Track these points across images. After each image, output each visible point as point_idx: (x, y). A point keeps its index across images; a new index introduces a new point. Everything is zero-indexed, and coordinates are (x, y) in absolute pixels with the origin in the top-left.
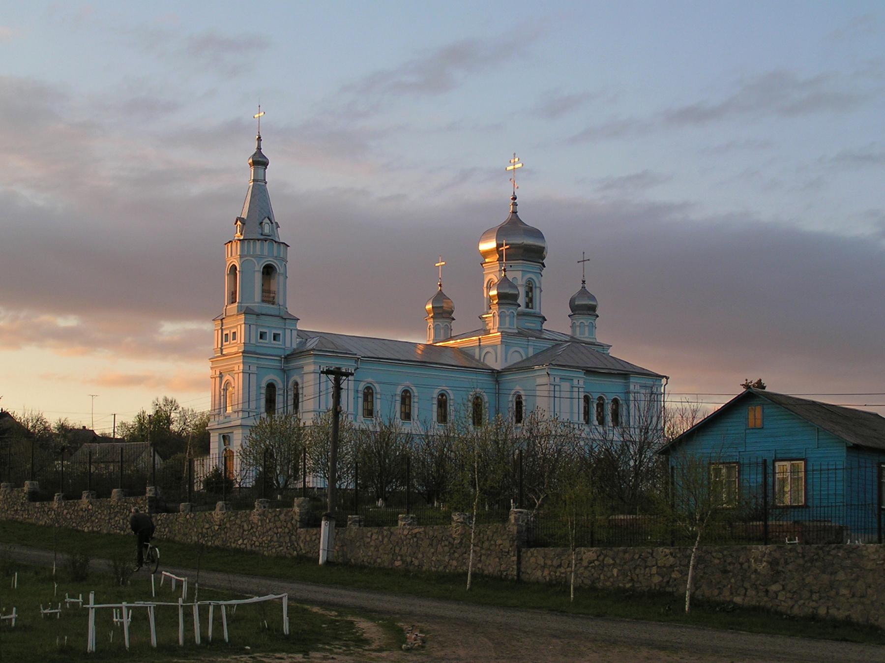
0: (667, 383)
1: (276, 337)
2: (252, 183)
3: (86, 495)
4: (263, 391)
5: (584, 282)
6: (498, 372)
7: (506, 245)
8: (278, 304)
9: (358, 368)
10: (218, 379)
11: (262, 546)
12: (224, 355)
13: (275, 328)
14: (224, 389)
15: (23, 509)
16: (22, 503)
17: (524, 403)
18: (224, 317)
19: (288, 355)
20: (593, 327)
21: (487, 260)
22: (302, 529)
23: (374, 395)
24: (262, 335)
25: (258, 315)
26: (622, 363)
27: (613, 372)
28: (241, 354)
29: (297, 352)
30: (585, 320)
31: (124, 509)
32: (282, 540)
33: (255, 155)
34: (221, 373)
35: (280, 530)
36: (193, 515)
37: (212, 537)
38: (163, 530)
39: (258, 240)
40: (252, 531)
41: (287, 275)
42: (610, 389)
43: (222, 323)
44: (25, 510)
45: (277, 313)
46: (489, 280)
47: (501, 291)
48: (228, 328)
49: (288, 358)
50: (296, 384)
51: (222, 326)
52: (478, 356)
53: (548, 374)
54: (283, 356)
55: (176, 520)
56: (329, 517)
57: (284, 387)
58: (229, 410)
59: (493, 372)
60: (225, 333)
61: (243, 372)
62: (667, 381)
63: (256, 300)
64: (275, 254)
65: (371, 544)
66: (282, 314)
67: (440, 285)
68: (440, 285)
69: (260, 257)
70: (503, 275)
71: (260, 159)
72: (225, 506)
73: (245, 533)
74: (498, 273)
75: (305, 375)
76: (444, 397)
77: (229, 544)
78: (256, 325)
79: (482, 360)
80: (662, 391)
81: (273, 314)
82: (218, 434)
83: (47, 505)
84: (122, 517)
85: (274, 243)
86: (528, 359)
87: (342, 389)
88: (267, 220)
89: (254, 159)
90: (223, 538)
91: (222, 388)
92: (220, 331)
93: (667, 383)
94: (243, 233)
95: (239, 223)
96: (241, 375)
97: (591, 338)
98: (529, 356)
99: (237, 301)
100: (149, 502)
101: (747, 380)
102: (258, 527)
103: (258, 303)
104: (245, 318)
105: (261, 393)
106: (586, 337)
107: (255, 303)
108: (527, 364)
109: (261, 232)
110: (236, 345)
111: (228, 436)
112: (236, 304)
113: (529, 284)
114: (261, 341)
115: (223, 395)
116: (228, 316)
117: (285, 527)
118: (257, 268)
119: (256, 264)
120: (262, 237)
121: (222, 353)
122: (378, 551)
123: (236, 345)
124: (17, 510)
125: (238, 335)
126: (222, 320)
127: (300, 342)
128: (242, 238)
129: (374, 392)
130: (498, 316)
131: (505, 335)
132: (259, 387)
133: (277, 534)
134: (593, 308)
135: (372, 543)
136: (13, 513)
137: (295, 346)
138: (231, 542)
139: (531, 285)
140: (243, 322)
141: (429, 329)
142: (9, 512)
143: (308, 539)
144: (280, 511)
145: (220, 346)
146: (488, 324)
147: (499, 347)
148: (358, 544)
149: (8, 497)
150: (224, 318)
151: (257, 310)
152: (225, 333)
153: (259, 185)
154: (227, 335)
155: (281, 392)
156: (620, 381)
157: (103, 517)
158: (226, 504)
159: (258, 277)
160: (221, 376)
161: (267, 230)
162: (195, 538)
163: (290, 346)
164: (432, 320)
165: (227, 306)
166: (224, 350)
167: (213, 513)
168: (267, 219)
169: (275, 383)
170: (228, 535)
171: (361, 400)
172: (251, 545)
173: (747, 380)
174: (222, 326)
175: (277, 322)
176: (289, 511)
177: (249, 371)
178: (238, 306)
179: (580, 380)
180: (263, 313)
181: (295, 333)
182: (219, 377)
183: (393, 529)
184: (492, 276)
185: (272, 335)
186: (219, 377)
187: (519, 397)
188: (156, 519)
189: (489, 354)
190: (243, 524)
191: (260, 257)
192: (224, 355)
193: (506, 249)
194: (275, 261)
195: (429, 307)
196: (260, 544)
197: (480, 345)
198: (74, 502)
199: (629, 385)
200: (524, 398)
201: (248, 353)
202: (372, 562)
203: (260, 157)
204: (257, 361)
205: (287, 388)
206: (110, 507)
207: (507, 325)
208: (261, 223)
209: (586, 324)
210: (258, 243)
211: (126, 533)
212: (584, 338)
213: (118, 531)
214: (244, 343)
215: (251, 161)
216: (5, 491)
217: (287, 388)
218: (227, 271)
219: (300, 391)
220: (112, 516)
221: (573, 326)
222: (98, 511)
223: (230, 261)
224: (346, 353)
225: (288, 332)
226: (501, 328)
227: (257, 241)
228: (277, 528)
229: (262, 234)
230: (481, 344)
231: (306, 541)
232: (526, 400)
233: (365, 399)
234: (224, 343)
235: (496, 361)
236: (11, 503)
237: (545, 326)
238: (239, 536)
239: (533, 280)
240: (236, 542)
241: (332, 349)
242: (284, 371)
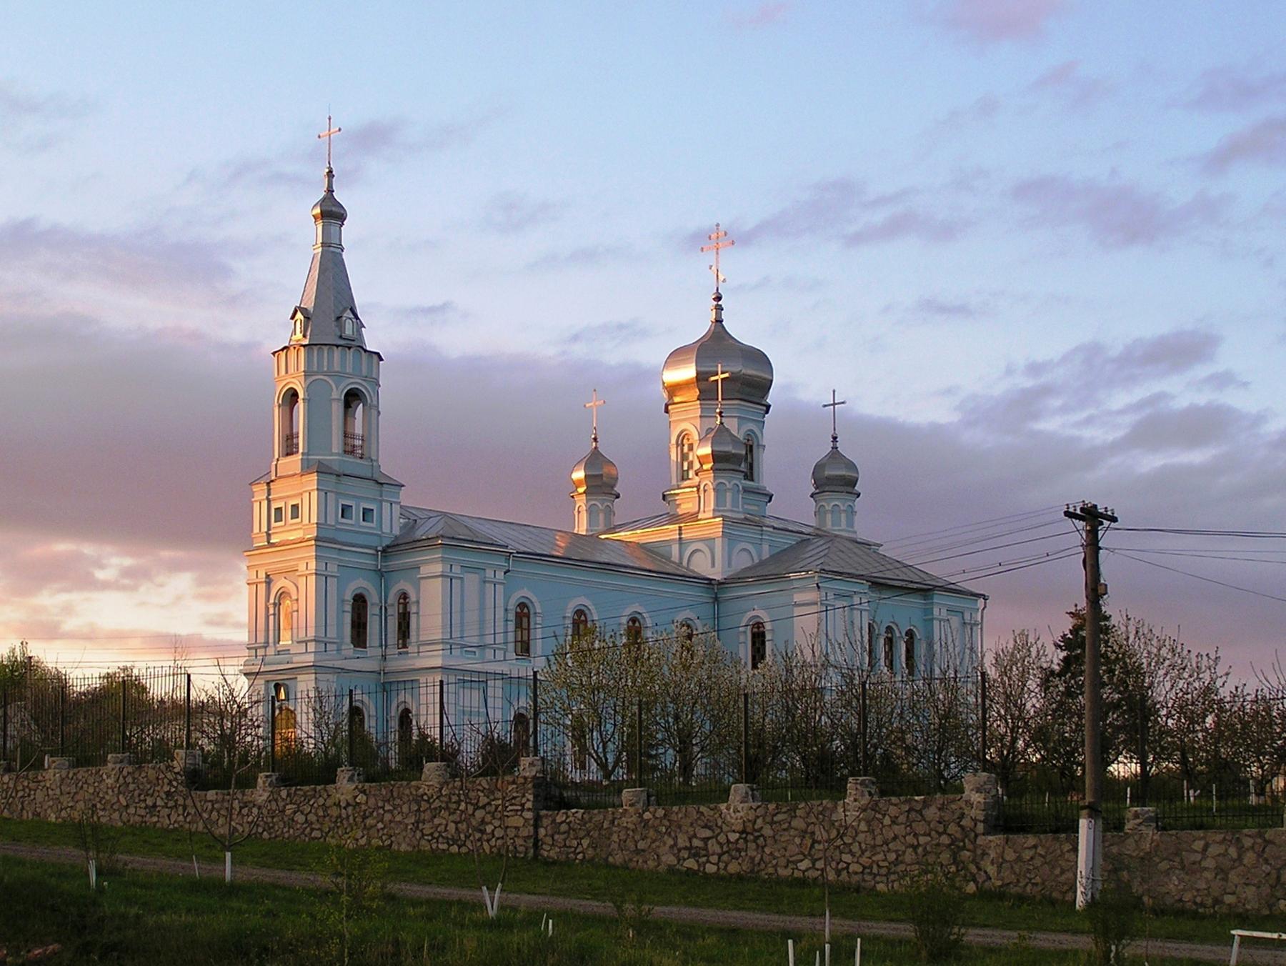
0: (985, 607)
1: (367, 513)
2: (320, 250)
3: (347, 776)
4: (348, 608)
5: (835, 438)
6: (720, 583)
7: (722, 373)
8: (370, 458)
9: (508, 571)
10: (262, 587)
11: (870, 873)
12: (273, 545)
13: (367, 499)
14: (275, 604)
15: (171, 804)
16: (168, 793)
17: (768, 637)
18: (273, 478)
19: (388, 547)
20: (852, 513)
21: (677, 399)
22: (990, 838)
23: (532, 616)
24: (345, 511)
25: (338, 476)
26: (919, 573)
27: (911, 586)
28: (313, 542)
29: (400, 542)
30: (834, 501)
31: (458, 803)
32: (931, 859)
33: (324, 200)
34: (268, 576)
35: (922, 840)
36: (660, 812)
37: (720, 856)
38: (575, 843)
39: (337, 346)
40: (839, 842)
41: (380, 409)
42: (903, 613)
43: (269, 490)
44: (176, 806)
45: (369, 475)
46: (682, 432)
47: (716, 449)
48: (281, 498)
49: (387, 552)
50: (404, 596)
51: (269, 494)
52: (677, 555)
53: (819, 587)
54: (380, 548)
55: (613, 822)
56: (1093, 811)
57: (381, 602)
58: (286, 641)
59: (710, 584)
60: (274, 505)
61: (316, 574)
62: (985, 603)
63: (334, 450)
64: (364, 372)
65: (1204, 864)
66: (375, 477)
67: (595, 439)
68: (595, 439)
69: (339, 376)
70: (718, 422)
71: (334, 209)
72: (750, 793)
73: (816, 846)
74: (699, 420)
75: (422, 582)
76: (637, 624)
77: (771, 870)
78: (337, 493)
79: (685, 563)
80: (979, 619)
81: (362, 475)
82: (263, 682)
83: (240, 796)
84: (451, 818)
85: (363, 352)
86: (762, 563)
87: (1100, 548)
88: (348, 314)
89: (324, 208)
90: (752, 859)
91: (272, 601)
92: (265, 504)
93: (985, 607)
94: (308, 333)
95: (299, 316)
96: (312, 579)
97: (849, 531)
98: (764, 558)
99: (301, 450)
100: (534, 786)
101: (1076, 606)
102: (857, 834)
103: (338, 454)
104: (318, 479)
105: (344, 611)
106: (842, 530)
107: (332, 454)
108: (772, 569)
109: (339, 334)
110: (300, 526)
111: (284, 684)
112: (297, 458)
113: (748, 440)
114: (344, 521)
115: (274, 614)
116: (281, 477)
117: (940, 834)
118: (335, 395)
119: (334, 386)
120: (342, 342)
121: (269, 542)
122: (1225, 879)
123: (300, 526)
124: (155, 806)
125: (305, 510)
126: (268, 484)
127: (405, 525)
128: (306, 342)
129: (532, 612)
130: (714, 489)
131: (728, 523)
132: (342, 601)
133: (915, 848)
134: (853, 482)
135: (1209, 863)
136: (143, 812)
137: (397, 531)
138: (775, 866)
139: (750, 443)
140: (316, 487)
141: (579, 512)
142: (132, 810)
143: (1010, 856)
144: (924, 801)
145: (264, 529)
146: (680, 505)
147: (718, 542)
148: (1164, 865)
149: (129, 780)
150: (272, 481)
151: (336, 468)
152: (274, 505)
153: (333, 252)
154: (279, 510)
155: (377, 611)
156: (917, 600)
157: (398, 818)
158: (753, 790)
159: (337, 409)
160: (269, 581)
161: (349, 330)
162: (669, 859)
163: (389, 531)
164: (584, 497)
165: (278, 460)
166: (272, 537)
167: (723, 807)
168: (349, 311)
169: (365, 593)
170: (767, 850)
171: (511, 626)
172: (838, 872)
173: (1076, 606)
174: (269, 494)
175: (369, 489)
176: (953, 801)
177: (325, 573)
178: (302, 459)
179: (863, 595)
180: (347, 472)
181: (396, 508)
182: (266, 582)
183: (1269, 834)
184: (686, 426)
185: (361, 510)
186: (266, 582)
187: (759, 625)
188: (554, 821)
189: (697, 555)
190: (810, 828)
191: (339, 376)
192: (273, 545)
193: (722, 379)
194: (364, 383)
195: (579, 475)
196: (864, 867)
197: (680, 538)
198: (315, 790)
199: (932, 608)
200: (768, 626)
201: (324, 541)
202: (1209, 902)
203: (334, 205)
204: (338, 555)
205: (386, 602)
206: (418, 799)
207: (728, 506)
208: (339, 318)
209: (842, 508)
210: (337, 352)
211: (464, 850)
212: (839, 530)
213: (445, 846)
214: (317, 523)
215: (318, 211)
216: (121, 771)
217: (386, 602)
218: (277, 399)
219: (413, 609)
220: (427, 816)
221: (819, 512)
222: (383, 808)
223: (284, 383)
224: (492, 545)
225: (386, 506)
226: (719, 511)
227: (335, 348)
228: (916, 835)
229: (341, 337)
230: (683, 536)
231: (1005, 861)
232: (772, 630)
233: (519, 625)
234: (273, 524)
235: (713, 565)
236: (136, 793)
237: (770, 509)
238: (803, 853)
239: (754, 433)
240: (791, 866)
241: (464, 535)
242: (381, 574)
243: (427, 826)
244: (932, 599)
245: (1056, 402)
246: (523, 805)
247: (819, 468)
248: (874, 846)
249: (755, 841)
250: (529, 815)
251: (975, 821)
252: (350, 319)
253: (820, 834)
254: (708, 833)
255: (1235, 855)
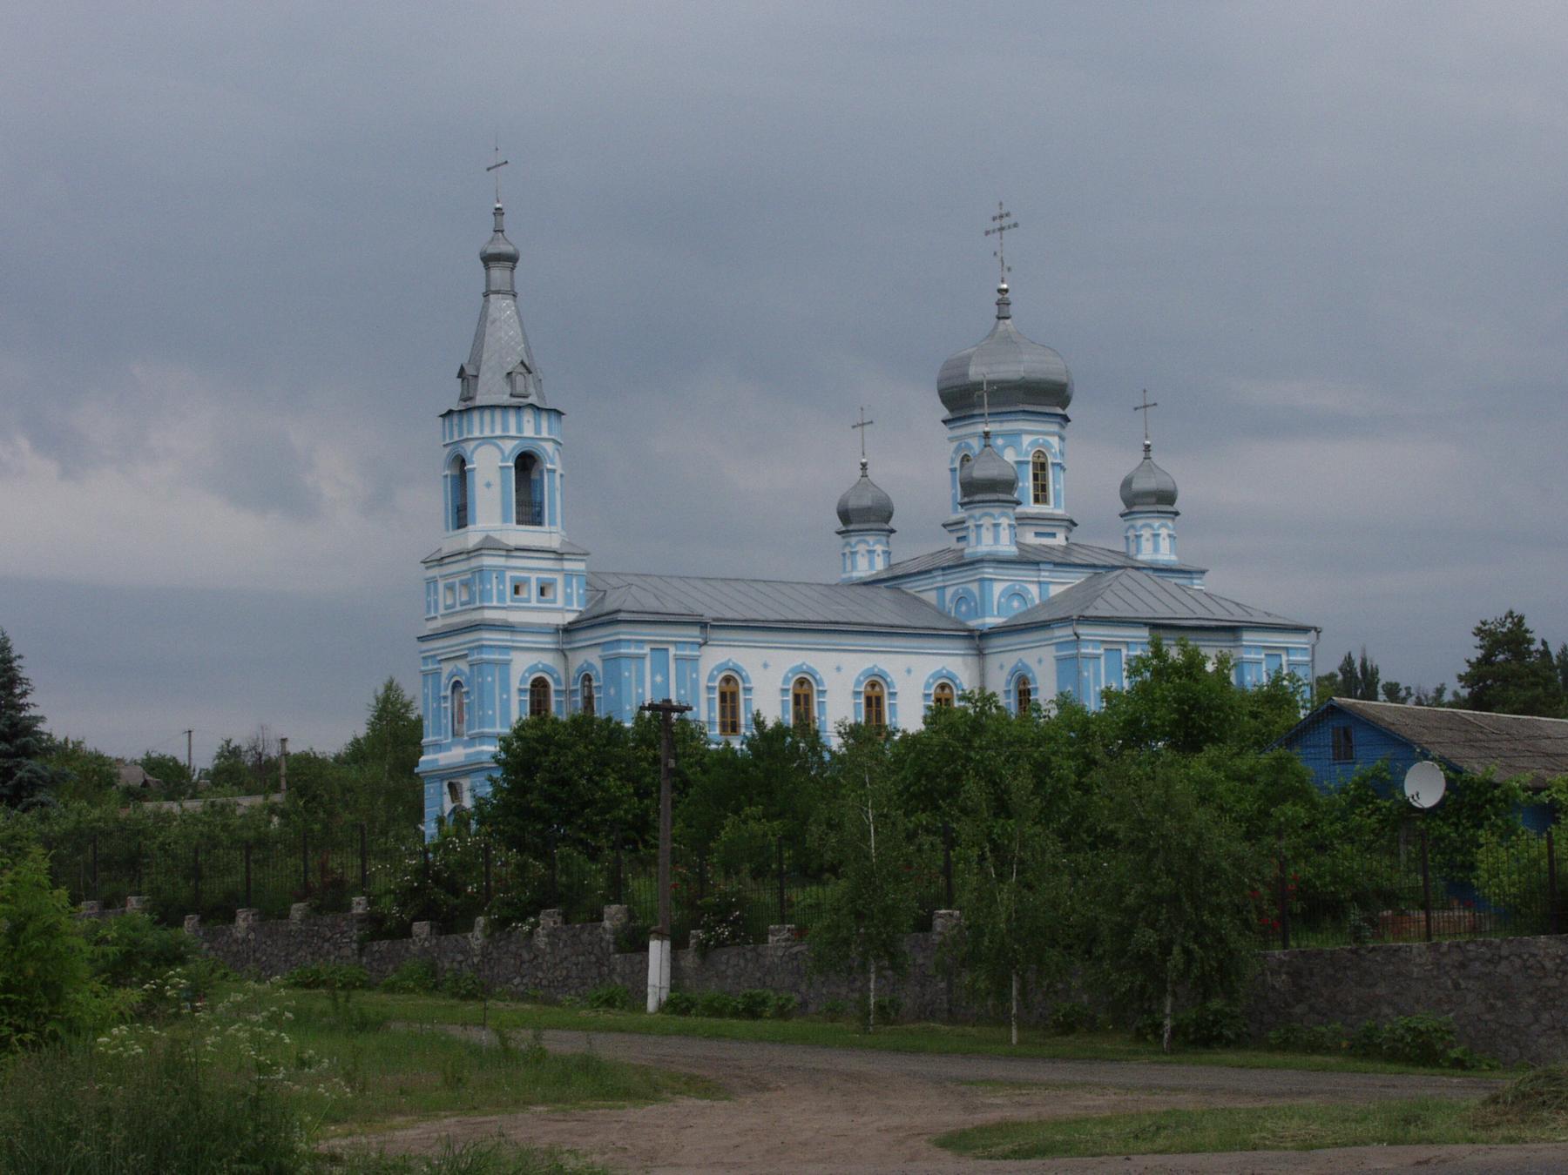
36: (434, 941)
133: (577, 965)
135: (730, 972)
139: (1042, 460)
167: (470, 935)
222: (265, 943)
243: (293, 958)
244: (1241, 640)
245: (659, 679)
246: (351, 937)
247: (1127, 484)
248: (556, 964)
249: (488, 962)
250: (354, 946)
251: (608, 942)
252: (521, 373)
253: (526, 956)
254: (460, 957)
255: (743, 965)
